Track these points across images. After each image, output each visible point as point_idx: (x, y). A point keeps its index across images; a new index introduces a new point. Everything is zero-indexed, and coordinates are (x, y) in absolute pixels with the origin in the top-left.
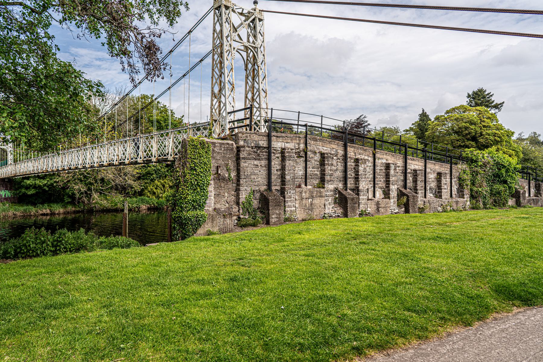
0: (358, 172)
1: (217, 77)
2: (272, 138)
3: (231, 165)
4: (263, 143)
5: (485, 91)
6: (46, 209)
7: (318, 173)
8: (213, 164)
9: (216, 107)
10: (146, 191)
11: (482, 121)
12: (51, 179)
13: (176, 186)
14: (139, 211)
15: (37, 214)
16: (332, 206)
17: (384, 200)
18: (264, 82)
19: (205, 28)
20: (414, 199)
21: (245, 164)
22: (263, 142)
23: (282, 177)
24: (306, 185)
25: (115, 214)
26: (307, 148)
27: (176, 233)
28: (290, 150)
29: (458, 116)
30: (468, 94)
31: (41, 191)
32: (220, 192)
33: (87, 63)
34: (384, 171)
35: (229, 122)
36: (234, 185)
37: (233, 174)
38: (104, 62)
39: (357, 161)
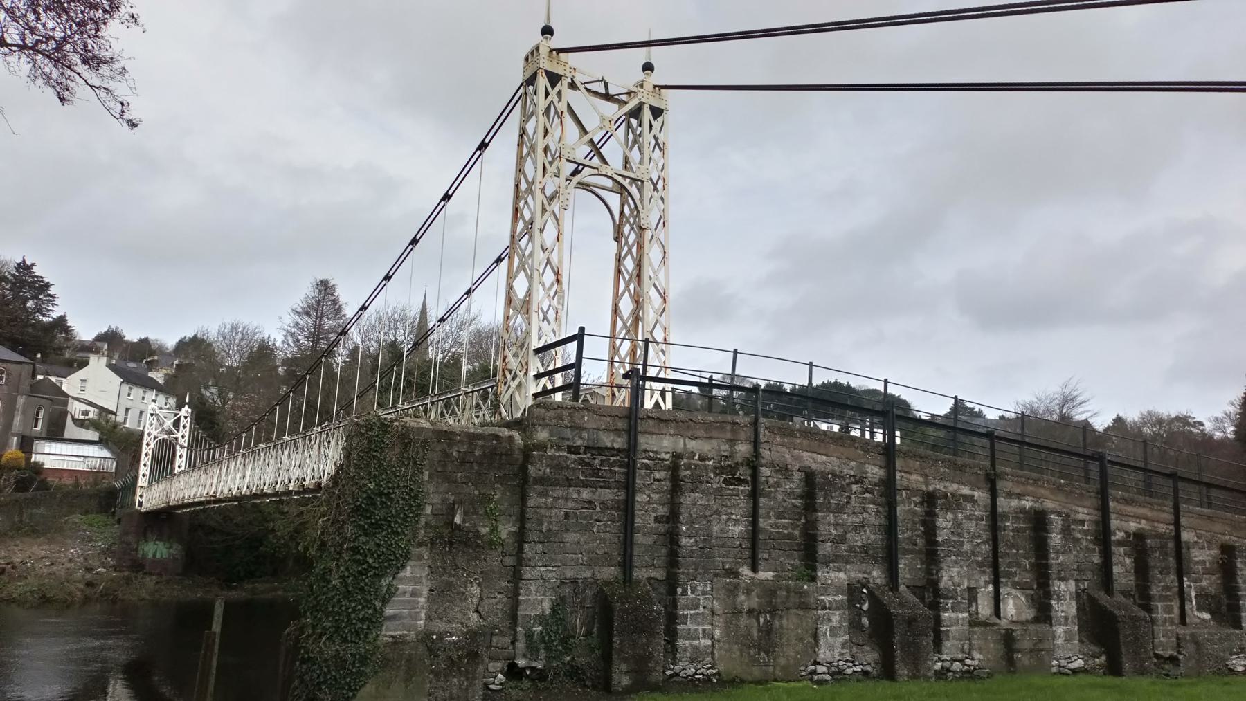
16: (840, 640)
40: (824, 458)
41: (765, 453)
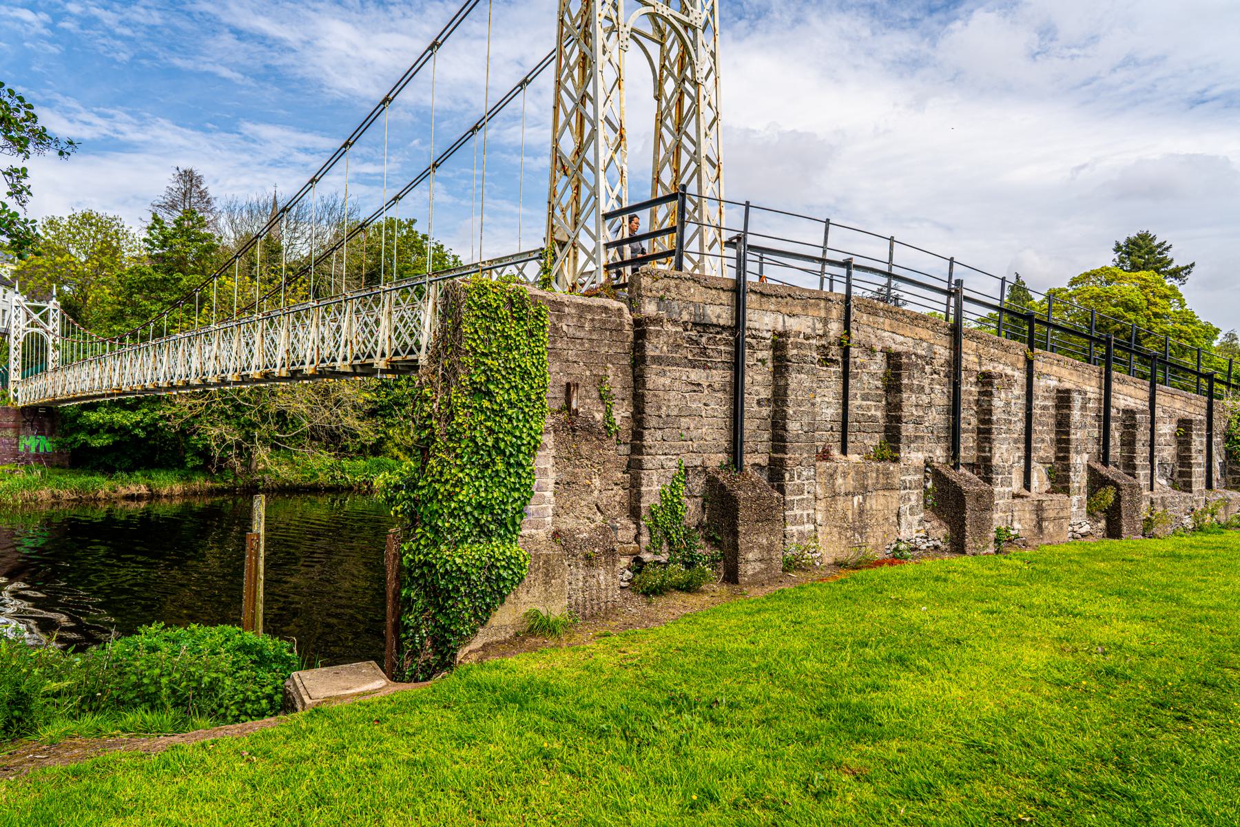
0: (990, 412)
1: (569, 105)
2: (748, 298)
3: (616, 381)
4: (720, 313)
5: (1154, 238)
6: (137, 483)
7: (879, 414)
8: (555, 375)
9: (564, 203)
10: (390, 445)
11: (1150, 303)
12: (152, 410)
13: (422, 450)
14: (370, 491)
15: (114, 495)
16: (917, 518)
17: (1054, 496)
18: (713, 133)
19: (539, 92)
20: (1132, 495)
21: (662, 380)
22: (718, 310)
23: (774, 425)
24: (844, 451)
25: (312, 497)
26: (848, 334)
27: (412, 623)
28: (801, 340)
29: (1097, 290)
30: (1118, 244)
31: (126, 438)
32: (575, 475)
34: (1053, 411)
35: (608, 246)
36: (624, 449)
37: (621, 413)
39: (986, 379)
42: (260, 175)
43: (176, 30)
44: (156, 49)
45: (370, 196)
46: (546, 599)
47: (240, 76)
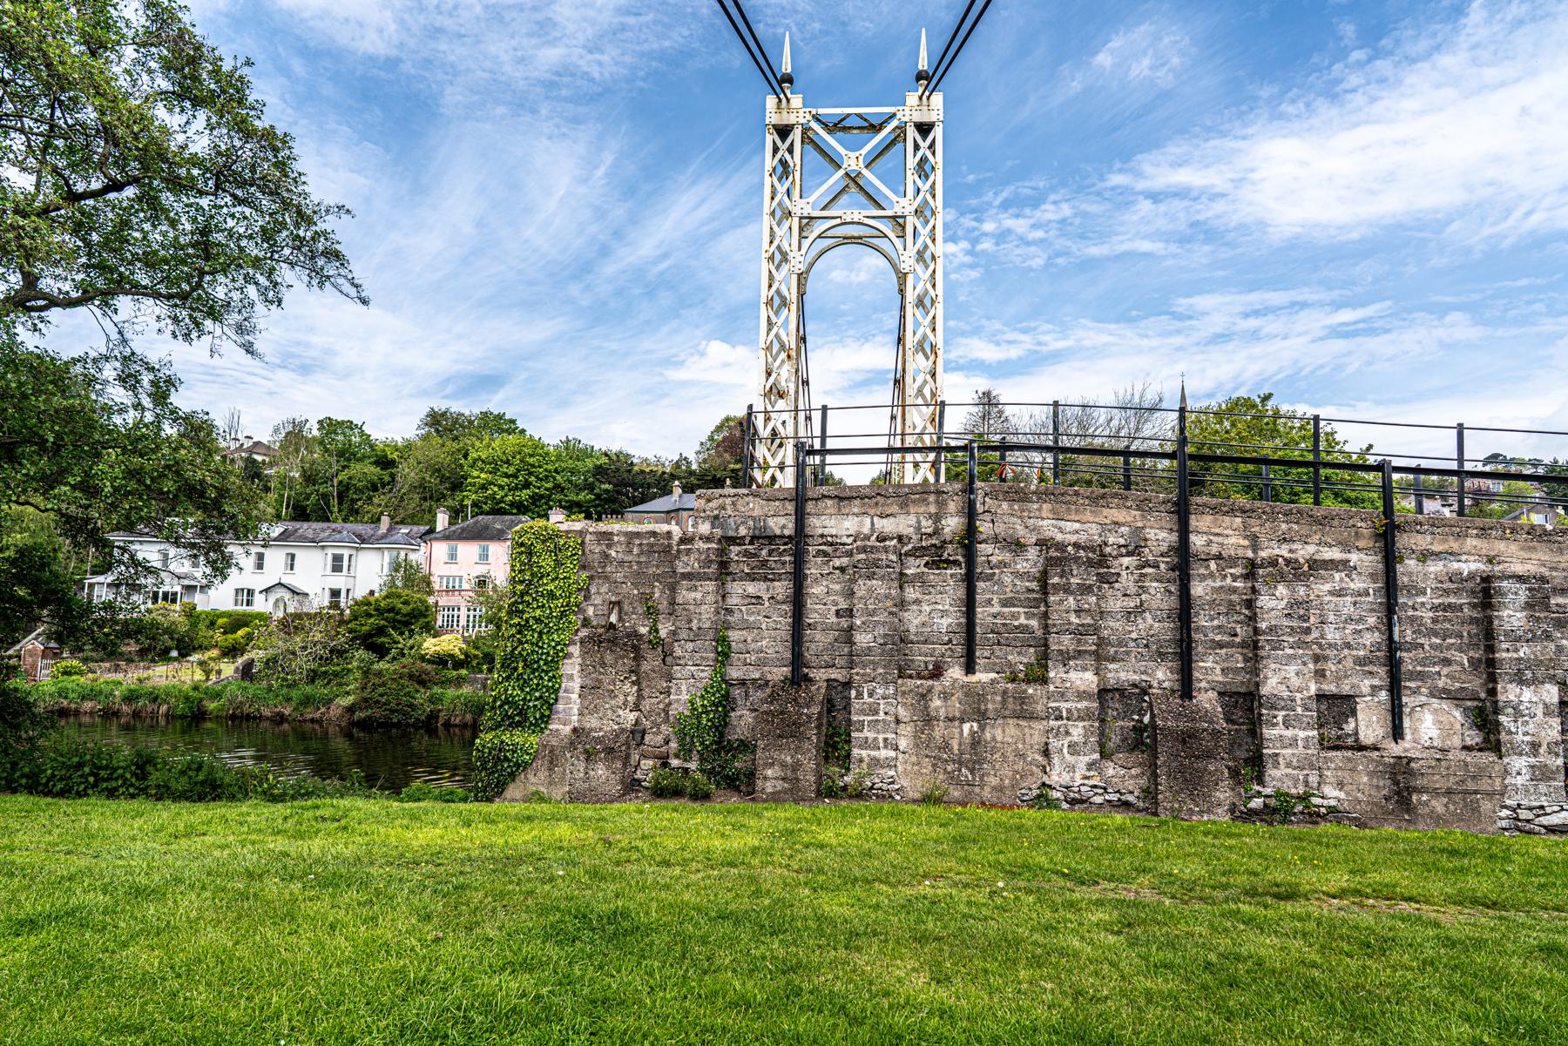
4: (782, 524)
21: (693, 595)
22: (782, 521)
32: (600, 681)
33: (1219, 330)
38: (1270, 317)
40: (1077, 526)
41: (984, 527)
42: (1200, 357)
43: (1085, 215)
44: (1069, 243)
45: (1350, 353)
46: (550, 783)
47: (1160, 245)
